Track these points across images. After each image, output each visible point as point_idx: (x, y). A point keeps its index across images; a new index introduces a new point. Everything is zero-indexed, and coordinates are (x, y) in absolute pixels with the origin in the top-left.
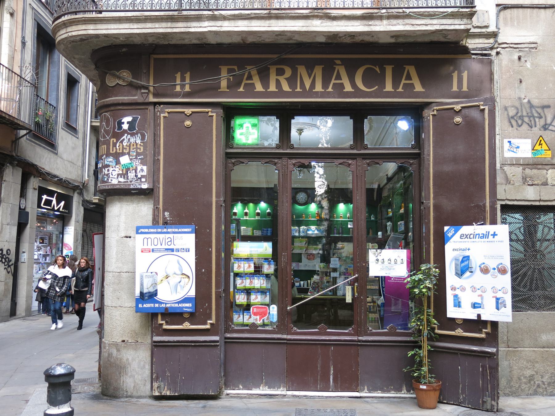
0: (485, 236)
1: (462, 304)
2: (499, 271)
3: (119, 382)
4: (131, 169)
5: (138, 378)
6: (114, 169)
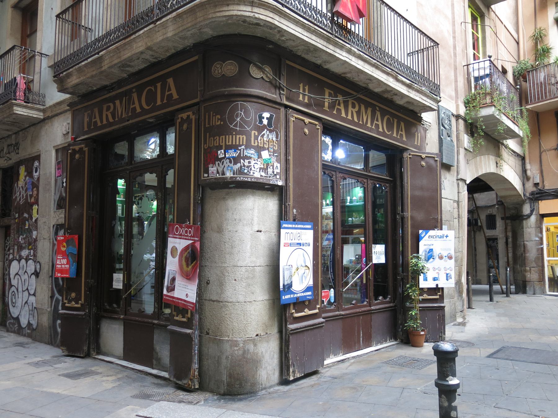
0: (441, 237)
1: (428, 279)
2: (448, 258)
3: (255, 377)
4: (270, 164)
5: (270, 368)
6: (256, 162)
